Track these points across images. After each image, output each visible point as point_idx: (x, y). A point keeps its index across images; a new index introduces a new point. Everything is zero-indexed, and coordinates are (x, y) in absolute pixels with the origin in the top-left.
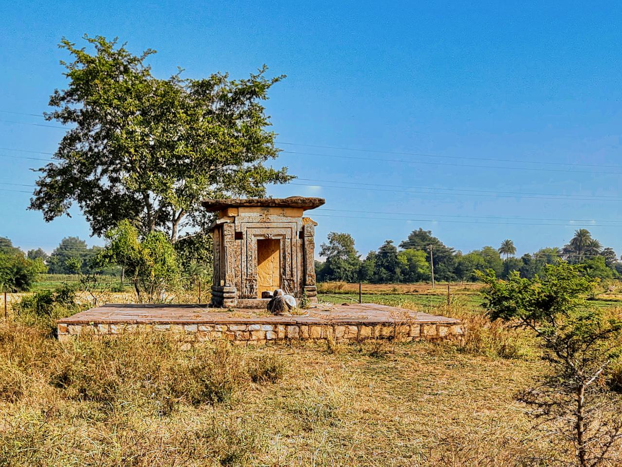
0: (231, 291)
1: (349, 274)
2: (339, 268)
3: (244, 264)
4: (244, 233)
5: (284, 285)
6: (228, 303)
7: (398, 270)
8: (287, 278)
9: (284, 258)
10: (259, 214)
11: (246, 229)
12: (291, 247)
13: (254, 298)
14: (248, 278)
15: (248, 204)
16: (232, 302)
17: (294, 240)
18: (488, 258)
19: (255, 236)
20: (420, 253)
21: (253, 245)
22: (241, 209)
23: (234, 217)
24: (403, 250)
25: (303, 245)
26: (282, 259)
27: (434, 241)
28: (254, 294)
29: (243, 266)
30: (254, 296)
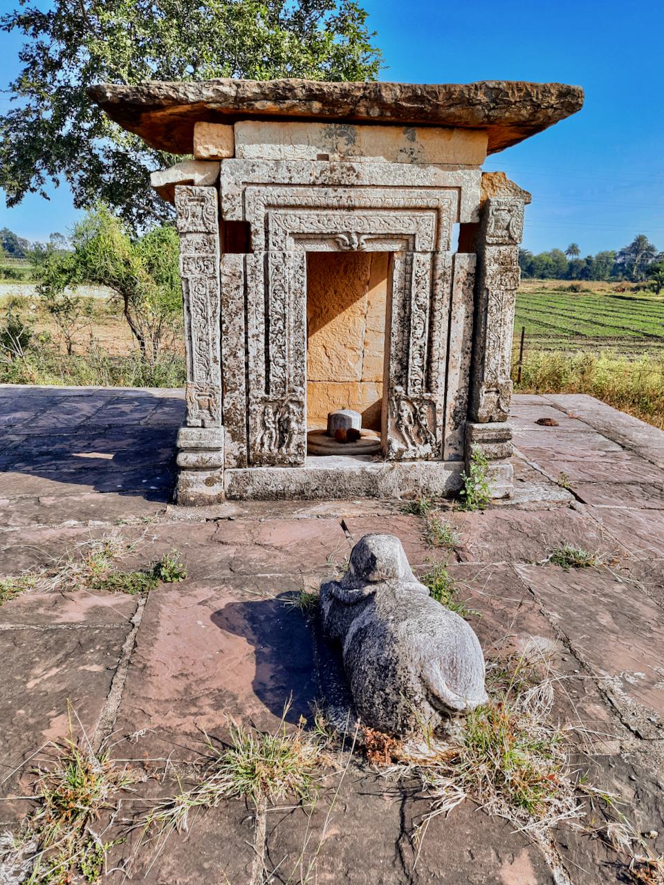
0: (205, 443)
3: (256, 346)
4: (257, 226)
5: (400, 417)
6: (193, 484)
8: (412, 395)
9: (406, 322)
10: (315, 151)
11: (262, 211)
12: (433, 285)
13: (292, 465)
14: (271, 397)
15: (269, 105)
16: (209, 482)
17: (445, 259)
18: (556, 258)
19: (300, 237)
21: (289, 274)
22: (243, 128)
23: (217, 160)
25: (478, 274)
26: (395, 327)
28: (292, 450)
29: (252, 352)
30: (292, 459)
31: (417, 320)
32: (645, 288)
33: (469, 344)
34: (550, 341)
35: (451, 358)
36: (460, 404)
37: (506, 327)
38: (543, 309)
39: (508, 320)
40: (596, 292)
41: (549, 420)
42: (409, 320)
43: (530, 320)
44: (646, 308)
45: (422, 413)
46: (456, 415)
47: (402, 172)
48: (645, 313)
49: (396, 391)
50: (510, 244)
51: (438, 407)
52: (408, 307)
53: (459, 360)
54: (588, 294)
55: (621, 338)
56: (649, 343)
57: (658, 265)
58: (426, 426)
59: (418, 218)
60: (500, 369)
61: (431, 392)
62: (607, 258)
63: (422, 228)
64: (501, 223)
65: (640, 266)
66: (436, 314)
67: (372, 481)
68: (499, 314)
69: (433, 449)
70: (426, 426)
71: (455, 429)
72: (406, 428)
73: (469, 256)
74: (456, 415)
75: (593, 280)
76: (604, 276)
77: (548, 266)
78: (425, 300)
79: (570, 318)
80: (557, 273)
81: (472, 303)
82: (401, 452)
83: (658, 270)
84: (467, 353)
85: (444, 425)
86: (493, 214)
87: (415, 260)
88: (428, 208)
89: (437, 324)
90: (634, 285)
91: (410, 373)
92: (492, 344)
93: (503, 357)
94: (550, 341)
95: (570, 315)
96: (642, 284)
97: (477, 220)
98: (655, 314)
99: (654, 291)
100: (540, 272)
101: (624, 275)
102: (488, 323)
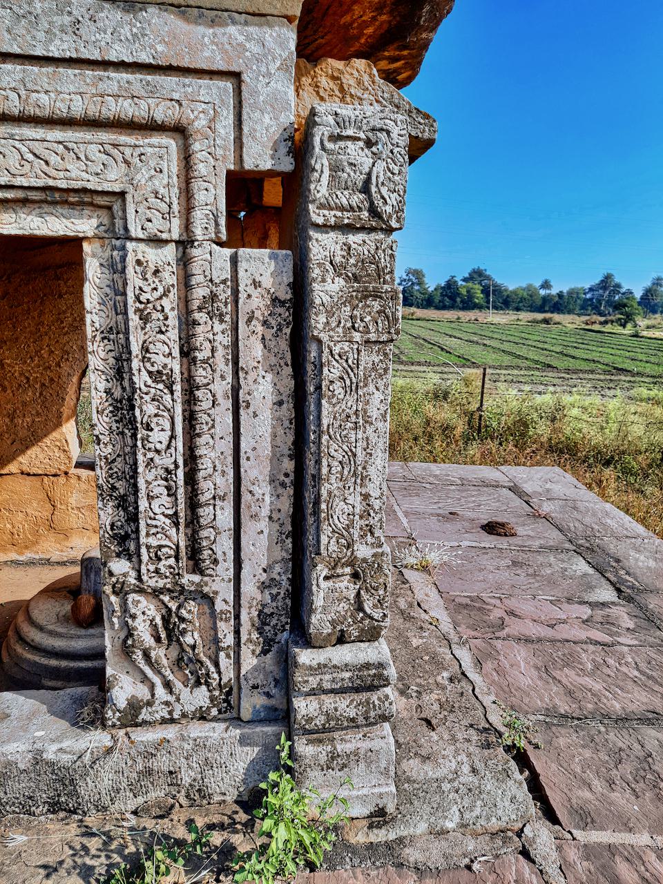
1: (420, 301)
2: (412, 296)
7: (458, 300)
8: (152, 582)
12: (188, 324)
20: (477, 286)
24: (464, 283)
27: (488, 278)
31: (151, 409)
32: (612, 322)
33: (289, 465)
34: (522, 372)
35: (246, 498)
36: (274, 598)
37: (370, 430)
38: (517, 340)
39: (374, 413)
40: (568, 325)
41: (503, 525)
42: (132, 408)
43: (503, 351)
44: (614, 341)
45: (182, 620)
46: (264, 624)
47: (67, 19)
48: (614, 346)
49: (111, 574)
50: (372, 230)
51: (219, 606)
52: (126, 376)
53: (264, 498)
54: (560, 326)
55: (592, 372)
56: (619, 377)
57: (625, 301)
58: (193, 647)
59: (128, 151)
60: (359, 523)
61: (202, 573)
62: (578, 293)
63: (142, 177)
64: (347, 174)
65: (607, 302)
66: (199, 394)
67: (61, 781)
68: (351, 400)
69: (212, 699)
70: (193, 647)
71: (265, 652)
72: (146, 655)
73: (273, 257)
74: (264, 624)
75: (564, 313)
76: (574, 309)
77: (522, 299)
78: (168, 361)
79: (542, 349)
80: (531, 306)
81: (289, 370)
82: (135, 705)
83: (625, 305)
84: (283, 485)
85: (238, 643)
86: (323, 148)
87: (131, 259)
88: (152, 127)
89: (203, 418)
90: (603, 319)
91: (143, 533)
92: (336, 468)
93: (366, 497)
94: (522, 372)
95: (542, 346)
96: (609, 318)
97: (287, 165)
98: (623, 348)
99: (621, 325)
100: (515, 305)
101: (593, 309)
102: (325, 422)
